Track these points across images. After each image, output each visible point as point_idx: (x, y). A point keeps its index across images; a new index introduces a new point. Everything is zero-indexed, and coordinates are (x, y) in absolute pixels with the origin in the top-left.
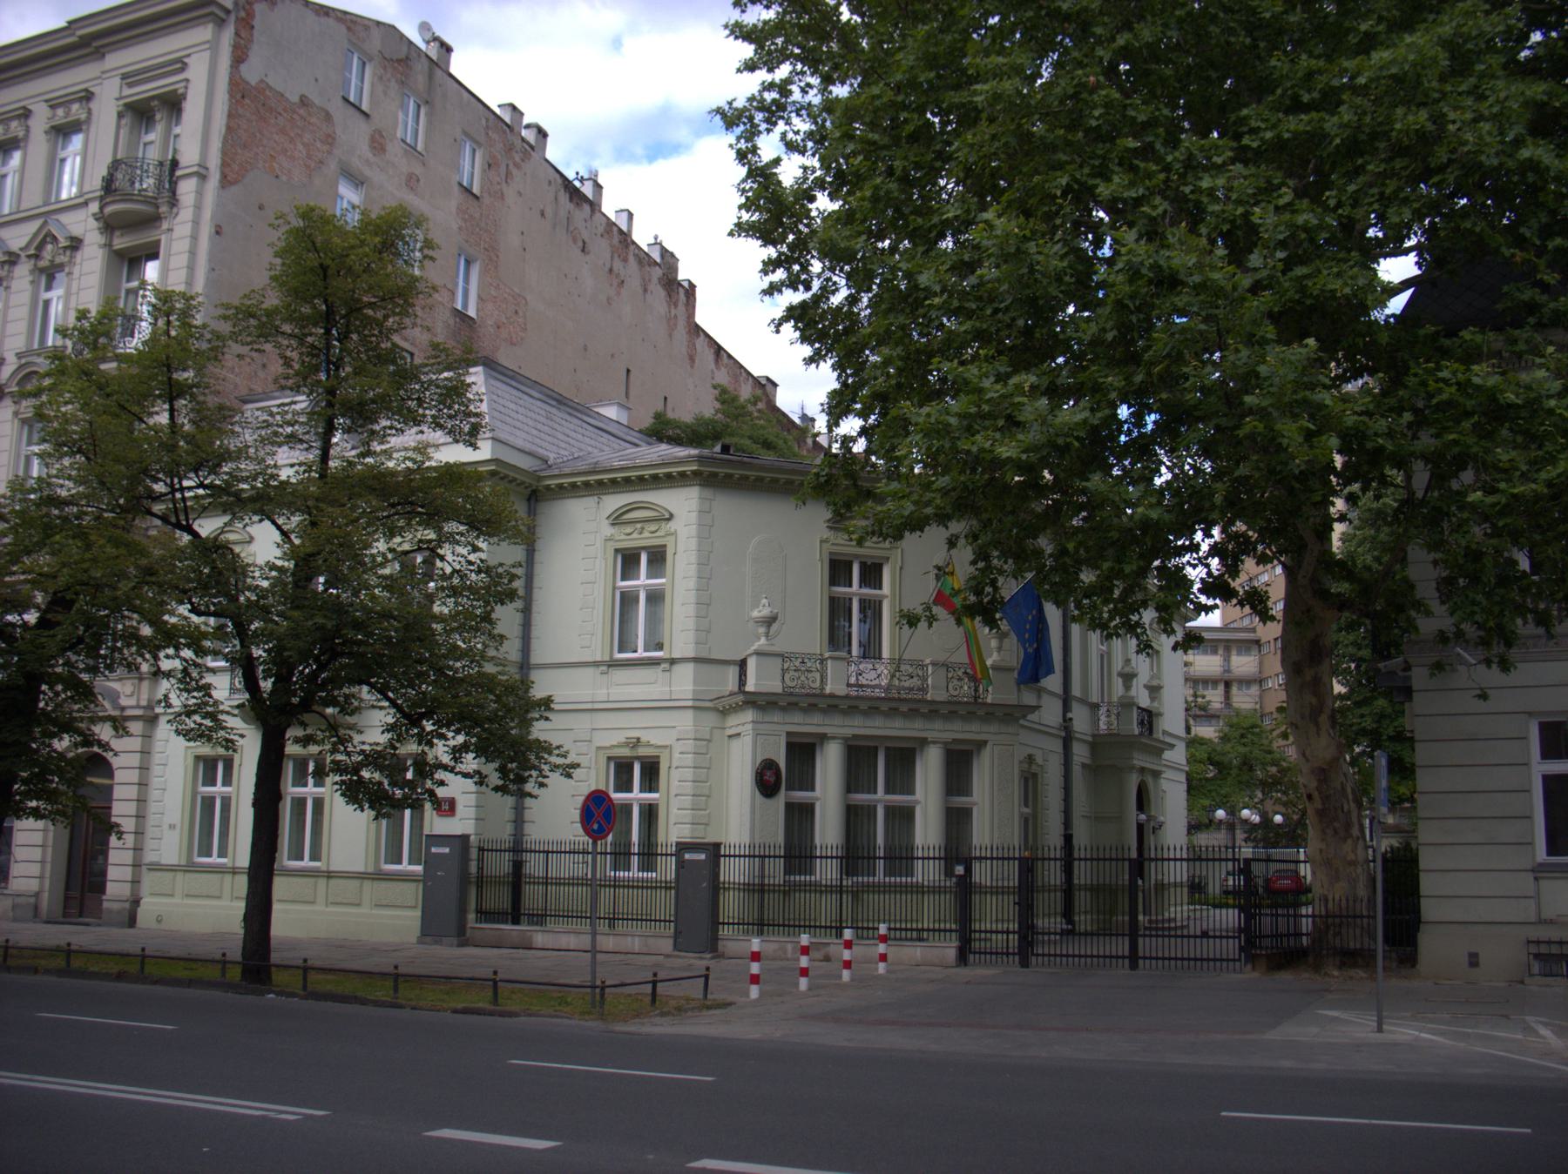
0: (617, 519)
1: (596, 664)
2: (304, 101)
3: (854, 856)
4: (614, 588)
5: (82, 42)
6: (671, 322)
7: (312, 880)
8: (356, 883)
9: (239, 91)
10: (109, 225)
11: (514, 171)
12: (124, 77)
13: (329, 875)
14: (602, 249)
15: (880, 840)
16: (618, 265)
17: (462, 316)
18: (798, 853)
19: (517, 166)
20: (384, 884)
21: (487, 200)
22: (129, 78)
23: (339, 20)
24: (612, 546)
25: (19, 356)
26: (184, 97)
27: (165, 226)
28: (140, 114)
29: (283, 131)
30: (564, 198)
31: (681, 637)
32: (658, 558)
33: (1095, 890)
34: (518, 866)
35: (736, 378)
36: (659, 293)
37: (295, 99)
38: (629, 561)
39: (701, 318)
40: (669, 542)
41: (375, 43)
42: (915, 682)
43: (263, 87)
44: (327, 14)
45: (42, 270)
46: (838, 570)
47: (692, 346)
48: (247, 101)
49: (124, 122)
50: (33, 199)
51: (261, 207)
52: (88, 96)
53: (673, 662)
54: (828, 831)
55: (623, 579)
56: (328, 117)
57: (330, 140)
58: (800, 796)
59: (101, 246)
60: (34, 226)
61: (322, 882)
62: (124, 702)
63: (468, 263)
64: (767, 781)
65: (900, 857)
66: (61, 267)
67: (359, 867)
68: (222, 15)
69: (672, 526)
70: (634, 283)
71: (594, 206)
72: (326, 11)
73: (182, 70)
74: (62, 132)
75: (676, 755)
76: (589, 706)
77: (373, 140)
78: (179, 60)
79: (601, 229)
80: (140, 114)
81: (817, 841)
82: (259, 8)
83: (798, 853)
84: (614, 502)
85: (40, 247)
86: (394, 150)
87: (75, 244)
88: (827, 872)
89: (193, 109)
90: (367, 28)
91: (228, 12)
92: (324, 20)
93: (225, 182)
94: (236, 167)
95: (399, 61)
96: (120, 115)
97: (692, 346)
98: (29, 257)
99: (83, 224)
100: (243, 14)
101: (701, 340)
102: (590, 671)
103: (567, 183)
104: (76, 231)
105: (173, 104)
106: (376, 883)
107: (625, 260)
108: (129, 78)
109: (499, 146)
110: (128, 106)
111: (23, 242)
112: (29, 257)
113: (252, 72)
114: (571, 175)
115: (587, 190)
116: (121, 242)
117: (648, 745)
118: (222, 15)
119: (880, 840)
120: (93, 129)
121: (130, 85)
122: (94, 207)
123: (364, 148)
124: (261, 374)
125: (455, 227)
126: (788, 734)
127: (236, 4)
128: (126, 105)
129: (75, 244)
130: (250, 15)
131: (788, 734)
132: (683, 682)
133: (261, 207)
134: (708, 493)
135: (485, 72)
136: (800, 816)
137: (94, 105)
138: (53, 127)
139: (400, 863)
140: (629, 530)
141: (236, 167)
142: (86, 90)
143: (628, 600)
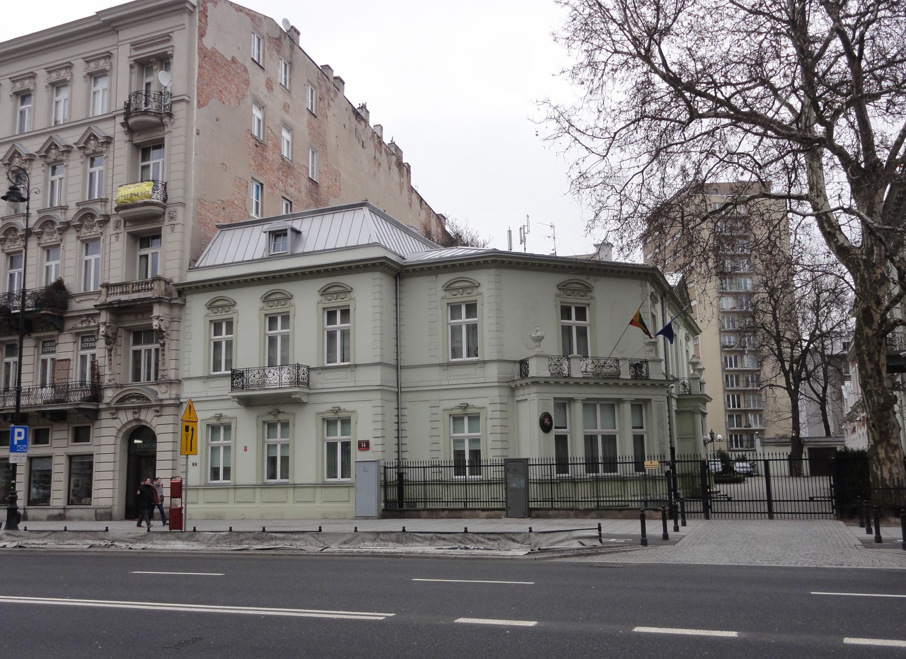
0: (448, 288)
1: (440, 365)
2: (234, 60)
3: (591, 464)
4: (265, 334)
5: (106, 24)
6: (401, 186)
7: (347, 489)
8: (251, 491)
9: (204, 54)
10: (131, 130)
11: (331, 102)
12: (132, 44)
13: (236, 487)
14: (370, 145)
15: (600, 454)
16: (378, 155)
17: (311, 180)
18: (562, 463)
19: (332, 99)
20: (329, 490)
21: (319, 117)
22: (136, 46)
23: (248, 14)
24: (445, 302)
25: (39, 212)
26: (171, 56)
27: (166, 130)
28: (144, 65)
29: (224, 77)
30: (353, 118)
31: (487, 348)
32: (472, 309)
33: (682, 476)
34: (400, 475)
35: (429, 215)
36: (395, 168)
37: (229, 59)
38: (331, 315)
39: (413, 184)
40: (479, 298)
41: (264, 29)
42: (614, 369)
43: (214, 52)
44: (241, 10)
45: (87, 156)
46: (565, 312)
47: (410, 198)
48: (207, 59)
49: (134, 70)
50: (78, 115)
51: (217, 120)
52: (108, 56)
53: (485, 362)
54: (577, 450)
55: (270, 330)
56: (246, 70)
57: (247, 82)
58: (561, 432)
59: (126, 142)
60: (82, 131)
61: (232, 492)
62: (161, 396)
63: (313, 153)
64: (546, 425)
65: (611, 463)
66: (101, 153)
67: (253, 481)
68: (191, 9)
69: (480, 290)
70: (385, 164)
71: (366, 121)
72: (240, 9)
73: (169, 40)
74: (94, 76)
75: (489, 412)
76: (438, 388)
77: (267, 83)
78: (168, 35)
79: (370, 135)
80: (144, 65)
81: (618, 454)
82: (210, 5)
83: (562, 463)
84: (445, 279)
85: (48, 151)
86: (277, 89)
87: (109, 141)
88: (580, 471)
89: (178, 63)
90: (260, 19)
91: (194, 7)
92: (240, 13)
93: (200, 105)
94: (204, 96)
95: (276, 39)
96: (131, 67)
97: (410, 198)
98: (80, 148)
99: (115, 129)
100: (202, 9)
101: (414, 196)
102: (438, 368)
103: (354, 110)
104: (109, 133)
105: (164, 61)
106: (324, 490)
107: (381, 152)
108: (136, 46)
109: (324, 89)
110: (136, 61)
111: (37, 148)
112: (80, 148)
113: (208, 42)
114: (356, 107)
115: (363, 114)
116: (138, 140)
117: (345, 411)
118: (191, 9)
119: (600, 454)
120: (114, 76)
121: (136, 49)
122: (121, 119)
123: (263, 88)
124: (222, 213)
125: (307, 133)
126: (555, 399)
127: (198, 3)
128: (135, 61)
129: (109, 141)
130: (205, 9)
131: (555, 399)
132: (492, 373)
133: (217, 120)
134: (499, 271)
135: (317, 47)
136: (561, 441)
137: (113, 60)
138: (88, 74)
139: (336, 477)
140: (455, 293)
141: (204, 96)
142: (108, 52)
143: (217, 345)
